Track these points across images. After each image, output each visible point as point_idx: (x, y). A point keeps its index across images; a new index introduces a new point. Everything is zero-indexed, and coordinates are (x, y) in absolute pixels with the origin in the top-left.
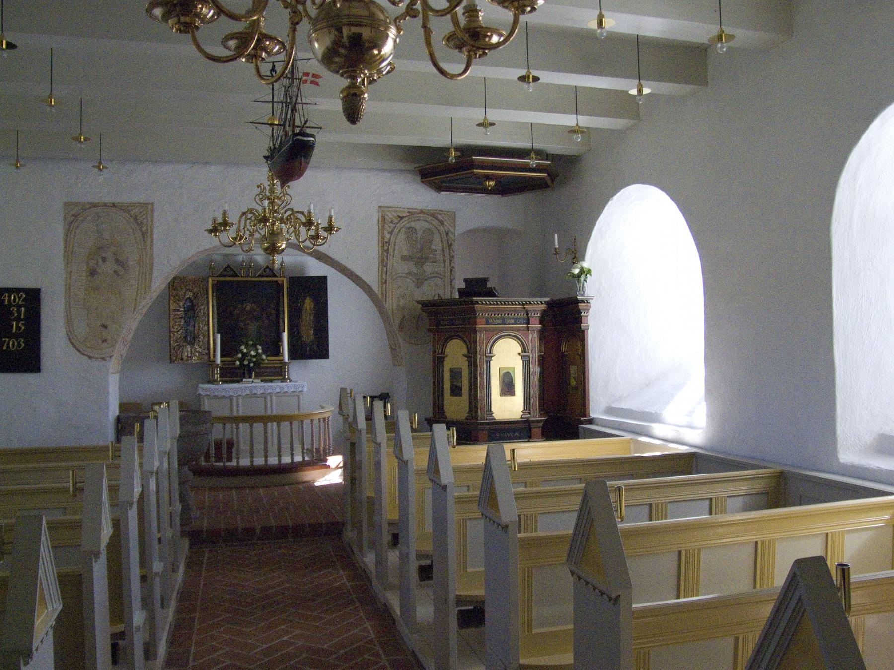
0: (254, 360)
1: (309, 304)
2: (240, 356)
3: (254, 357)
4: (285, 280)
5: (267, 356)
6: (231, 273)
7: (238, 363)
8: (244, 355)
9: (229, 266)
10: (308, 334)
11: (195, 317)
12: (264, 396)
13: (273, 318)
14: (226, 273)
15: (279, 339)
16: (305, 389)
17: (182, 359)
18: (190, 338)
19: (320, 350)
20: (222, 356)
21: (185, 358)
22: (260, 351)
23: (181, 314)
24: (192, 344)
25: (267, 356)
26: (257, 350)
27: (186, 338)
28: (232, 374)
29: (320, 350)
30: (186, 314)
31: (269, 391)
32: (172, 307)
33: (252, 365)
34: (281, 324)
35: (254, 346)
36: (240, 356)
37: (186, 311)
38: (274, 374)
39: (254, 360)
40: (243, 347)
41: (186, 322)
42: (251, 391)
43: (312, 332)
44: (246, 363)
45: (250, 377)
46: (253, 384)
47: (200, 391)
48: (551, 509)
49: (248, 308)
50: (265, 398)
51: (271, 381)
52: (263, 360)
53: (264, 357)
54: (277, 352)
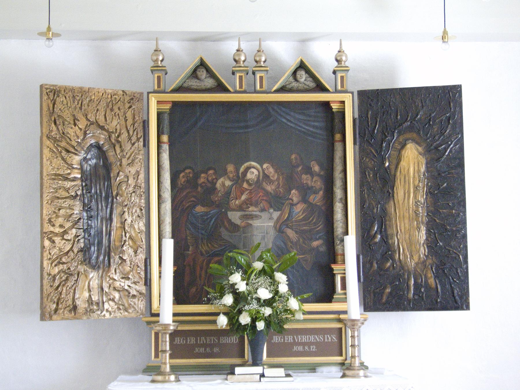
0: (267, 311)
1: (412, 161)
2: (228, 300)
3: (268, 303)
4: (348, 99)
6: (210, 83)
7: (223, 321)
8: (239, 297)
9: (202, 64)
10: (411, 240)
11: (109, 198)
13: (317, 199)
14: (194, 83)
18: (98, 251)
19: (443, 285)
21: (82, 304)
22: (283, 288)
23: (75, 186)
24: (103, 266)
25: (303, 301)
26: (274, 283)
27: (85, 251)
30: (87, 188)
33: (261, 325)
35: (267, 273)
36: (228, 300)
37: (89, 179)
39: (267, 311)
40: (236, 278)
41: (86, 207)
43: (422, 235)
44: (245, 319)
45: (256, 363)
48: (145, 108)
49: (252, 175)
53: (294, 303)
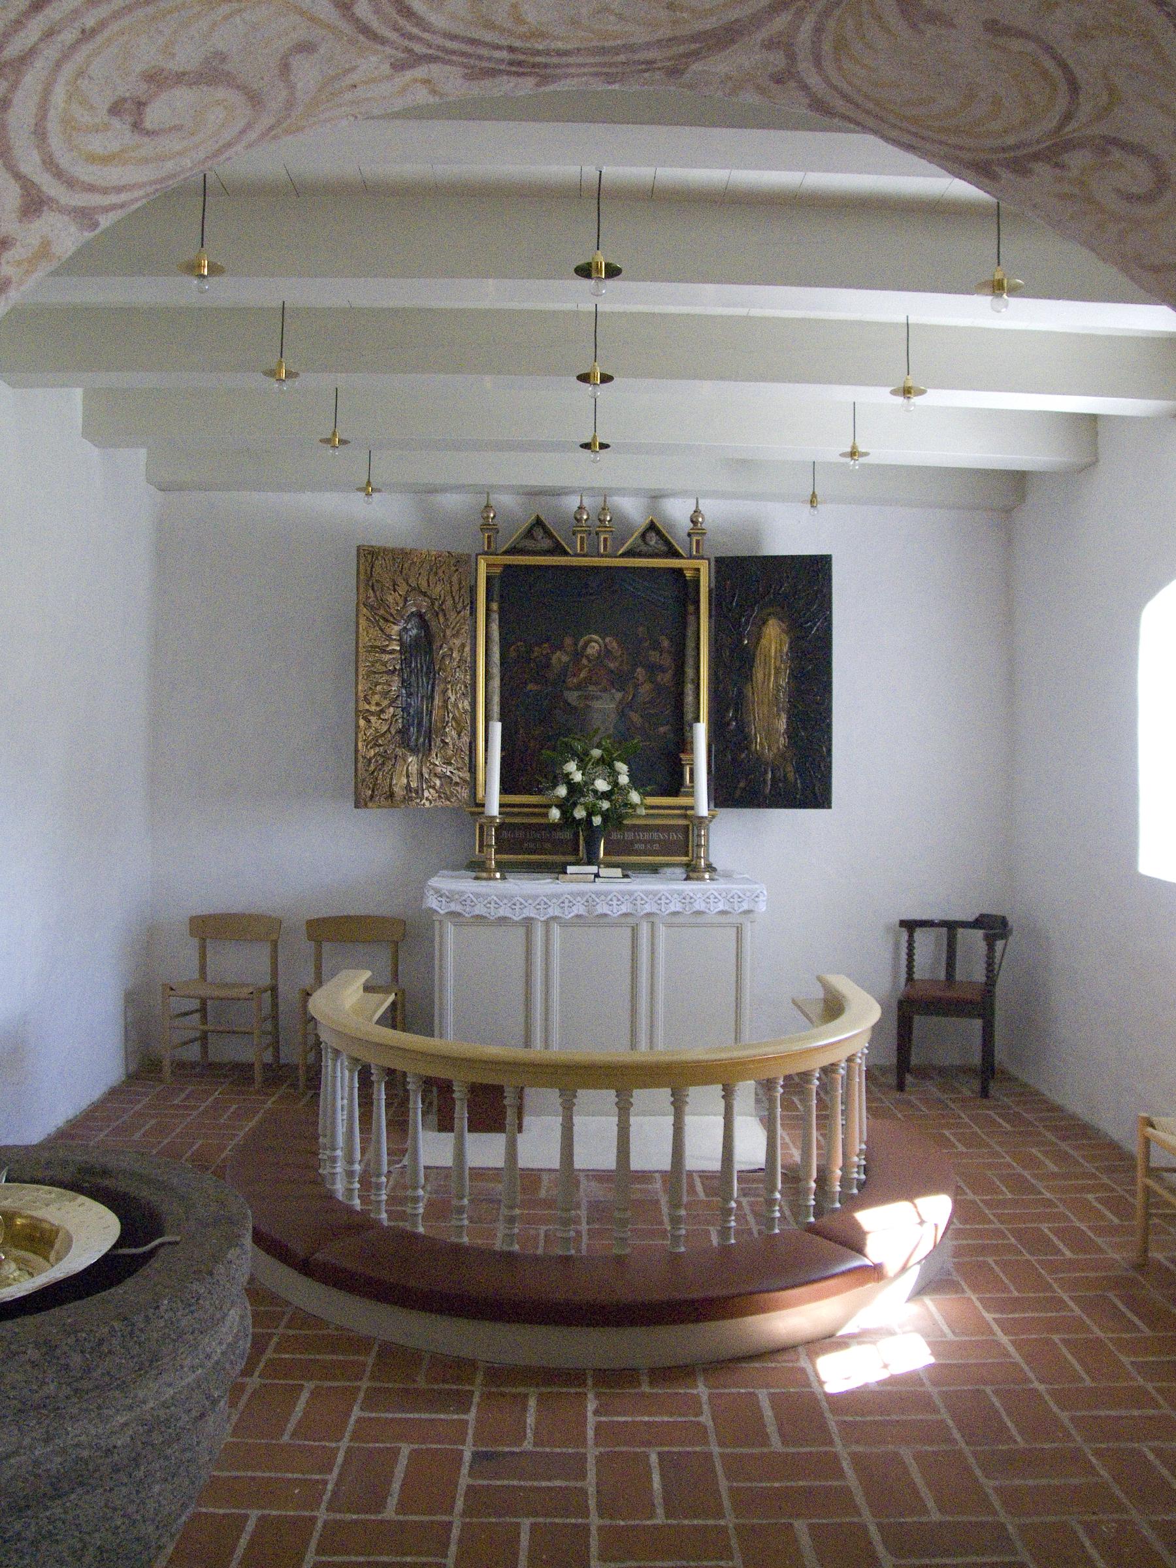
0: (605, 805)
1: (774, 639)
2: (562, 791)
3: (606, 796)
4: (704, 566)
5: (644, 794)
7: (555, 814)
8: (573, 788)
9: (539, 522)
10: (770, 729)
12: (631, 924)
13: (666, 678)
14: (529, 544)
15: (684, 744)
16: (762, 907)
17: (391, 795)
18: (417, 733)
19: (803, 780)
20: (505, 789)
21: (399, 791)
22: (624, 779)
23: (392, 660)
24: (423, 750)
26: (614, 774)
27: (403, 732)
28: (536, 844)
29: (803, 780)
30: (406, 662)
31: (648, 908)
32: (364, 639)
33: (597, 820)
34: (689, 699)
35: (607, 762)
36: (562, 791)
37: (409, 650)
38: (668, 849)
39: (605, 805)
40: (571, 766)
41: (405, 683)
42: (590, 903)
43: (782, 724)
44: (580, 813)
46: (599, 886)
47: (432, 902)
49: (593, 649)
50: (634, 930)
51: (654, 869)
52: (634, 807)
53: (635, 797)
54: (673, 781)
